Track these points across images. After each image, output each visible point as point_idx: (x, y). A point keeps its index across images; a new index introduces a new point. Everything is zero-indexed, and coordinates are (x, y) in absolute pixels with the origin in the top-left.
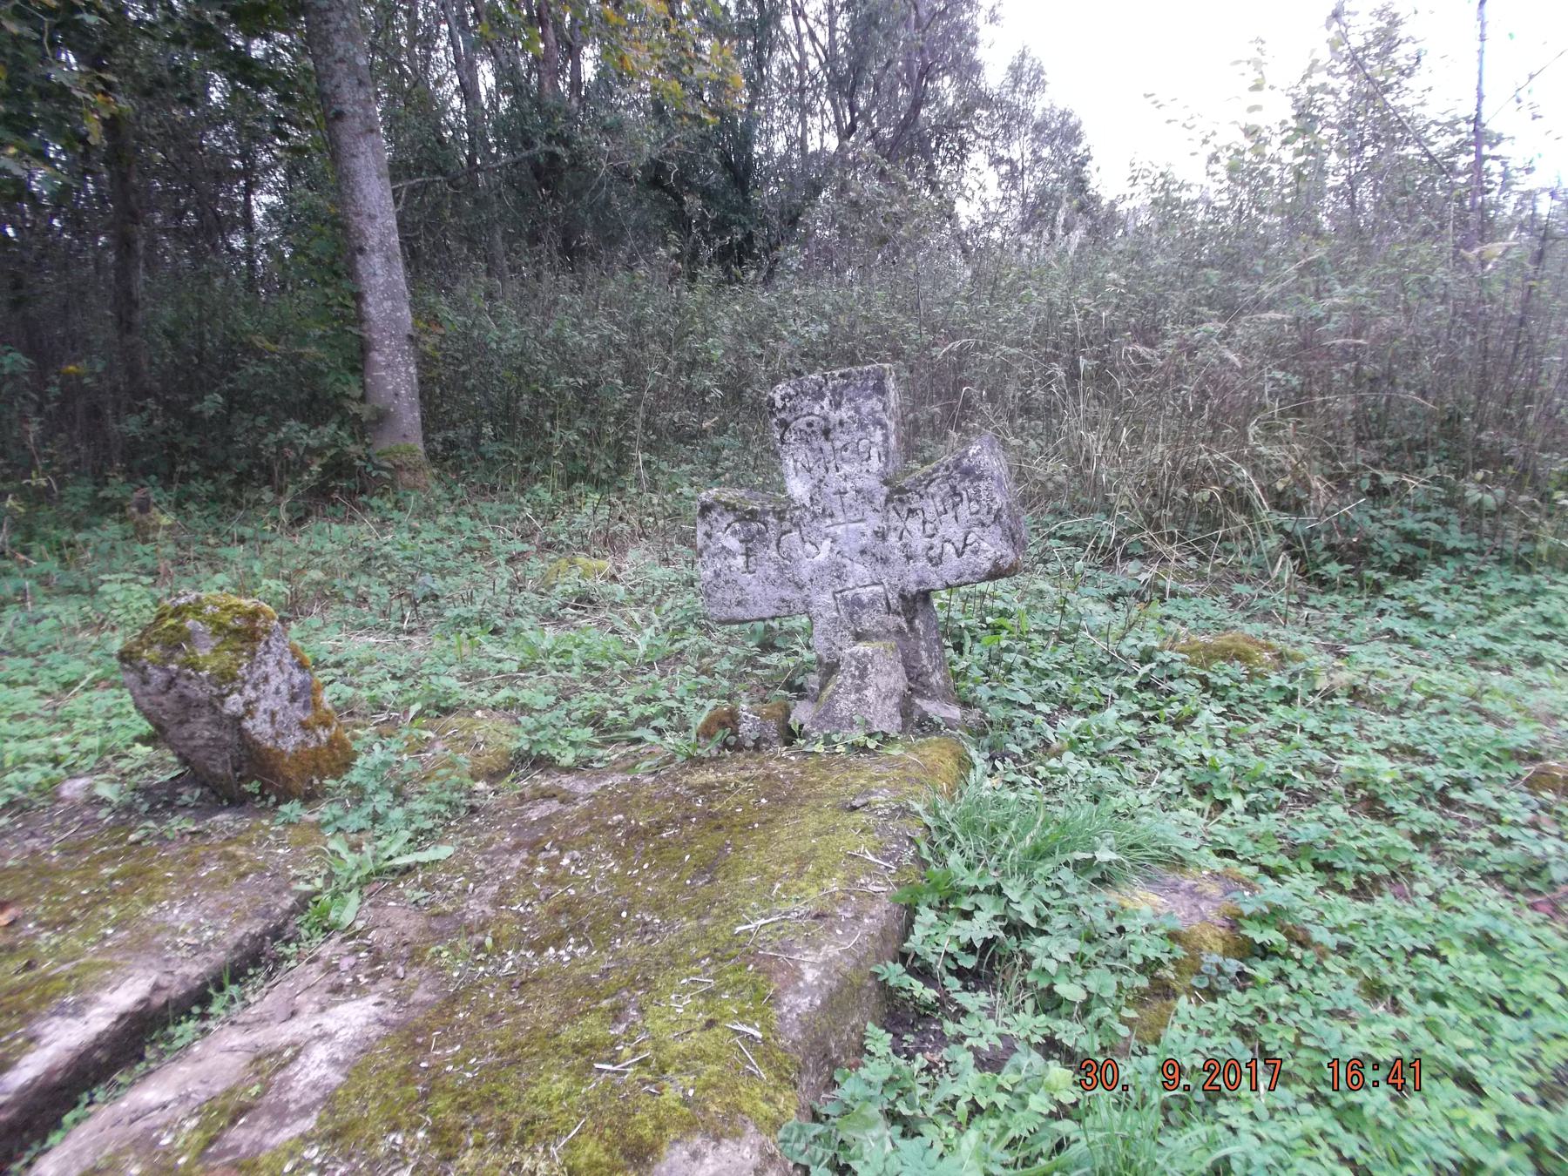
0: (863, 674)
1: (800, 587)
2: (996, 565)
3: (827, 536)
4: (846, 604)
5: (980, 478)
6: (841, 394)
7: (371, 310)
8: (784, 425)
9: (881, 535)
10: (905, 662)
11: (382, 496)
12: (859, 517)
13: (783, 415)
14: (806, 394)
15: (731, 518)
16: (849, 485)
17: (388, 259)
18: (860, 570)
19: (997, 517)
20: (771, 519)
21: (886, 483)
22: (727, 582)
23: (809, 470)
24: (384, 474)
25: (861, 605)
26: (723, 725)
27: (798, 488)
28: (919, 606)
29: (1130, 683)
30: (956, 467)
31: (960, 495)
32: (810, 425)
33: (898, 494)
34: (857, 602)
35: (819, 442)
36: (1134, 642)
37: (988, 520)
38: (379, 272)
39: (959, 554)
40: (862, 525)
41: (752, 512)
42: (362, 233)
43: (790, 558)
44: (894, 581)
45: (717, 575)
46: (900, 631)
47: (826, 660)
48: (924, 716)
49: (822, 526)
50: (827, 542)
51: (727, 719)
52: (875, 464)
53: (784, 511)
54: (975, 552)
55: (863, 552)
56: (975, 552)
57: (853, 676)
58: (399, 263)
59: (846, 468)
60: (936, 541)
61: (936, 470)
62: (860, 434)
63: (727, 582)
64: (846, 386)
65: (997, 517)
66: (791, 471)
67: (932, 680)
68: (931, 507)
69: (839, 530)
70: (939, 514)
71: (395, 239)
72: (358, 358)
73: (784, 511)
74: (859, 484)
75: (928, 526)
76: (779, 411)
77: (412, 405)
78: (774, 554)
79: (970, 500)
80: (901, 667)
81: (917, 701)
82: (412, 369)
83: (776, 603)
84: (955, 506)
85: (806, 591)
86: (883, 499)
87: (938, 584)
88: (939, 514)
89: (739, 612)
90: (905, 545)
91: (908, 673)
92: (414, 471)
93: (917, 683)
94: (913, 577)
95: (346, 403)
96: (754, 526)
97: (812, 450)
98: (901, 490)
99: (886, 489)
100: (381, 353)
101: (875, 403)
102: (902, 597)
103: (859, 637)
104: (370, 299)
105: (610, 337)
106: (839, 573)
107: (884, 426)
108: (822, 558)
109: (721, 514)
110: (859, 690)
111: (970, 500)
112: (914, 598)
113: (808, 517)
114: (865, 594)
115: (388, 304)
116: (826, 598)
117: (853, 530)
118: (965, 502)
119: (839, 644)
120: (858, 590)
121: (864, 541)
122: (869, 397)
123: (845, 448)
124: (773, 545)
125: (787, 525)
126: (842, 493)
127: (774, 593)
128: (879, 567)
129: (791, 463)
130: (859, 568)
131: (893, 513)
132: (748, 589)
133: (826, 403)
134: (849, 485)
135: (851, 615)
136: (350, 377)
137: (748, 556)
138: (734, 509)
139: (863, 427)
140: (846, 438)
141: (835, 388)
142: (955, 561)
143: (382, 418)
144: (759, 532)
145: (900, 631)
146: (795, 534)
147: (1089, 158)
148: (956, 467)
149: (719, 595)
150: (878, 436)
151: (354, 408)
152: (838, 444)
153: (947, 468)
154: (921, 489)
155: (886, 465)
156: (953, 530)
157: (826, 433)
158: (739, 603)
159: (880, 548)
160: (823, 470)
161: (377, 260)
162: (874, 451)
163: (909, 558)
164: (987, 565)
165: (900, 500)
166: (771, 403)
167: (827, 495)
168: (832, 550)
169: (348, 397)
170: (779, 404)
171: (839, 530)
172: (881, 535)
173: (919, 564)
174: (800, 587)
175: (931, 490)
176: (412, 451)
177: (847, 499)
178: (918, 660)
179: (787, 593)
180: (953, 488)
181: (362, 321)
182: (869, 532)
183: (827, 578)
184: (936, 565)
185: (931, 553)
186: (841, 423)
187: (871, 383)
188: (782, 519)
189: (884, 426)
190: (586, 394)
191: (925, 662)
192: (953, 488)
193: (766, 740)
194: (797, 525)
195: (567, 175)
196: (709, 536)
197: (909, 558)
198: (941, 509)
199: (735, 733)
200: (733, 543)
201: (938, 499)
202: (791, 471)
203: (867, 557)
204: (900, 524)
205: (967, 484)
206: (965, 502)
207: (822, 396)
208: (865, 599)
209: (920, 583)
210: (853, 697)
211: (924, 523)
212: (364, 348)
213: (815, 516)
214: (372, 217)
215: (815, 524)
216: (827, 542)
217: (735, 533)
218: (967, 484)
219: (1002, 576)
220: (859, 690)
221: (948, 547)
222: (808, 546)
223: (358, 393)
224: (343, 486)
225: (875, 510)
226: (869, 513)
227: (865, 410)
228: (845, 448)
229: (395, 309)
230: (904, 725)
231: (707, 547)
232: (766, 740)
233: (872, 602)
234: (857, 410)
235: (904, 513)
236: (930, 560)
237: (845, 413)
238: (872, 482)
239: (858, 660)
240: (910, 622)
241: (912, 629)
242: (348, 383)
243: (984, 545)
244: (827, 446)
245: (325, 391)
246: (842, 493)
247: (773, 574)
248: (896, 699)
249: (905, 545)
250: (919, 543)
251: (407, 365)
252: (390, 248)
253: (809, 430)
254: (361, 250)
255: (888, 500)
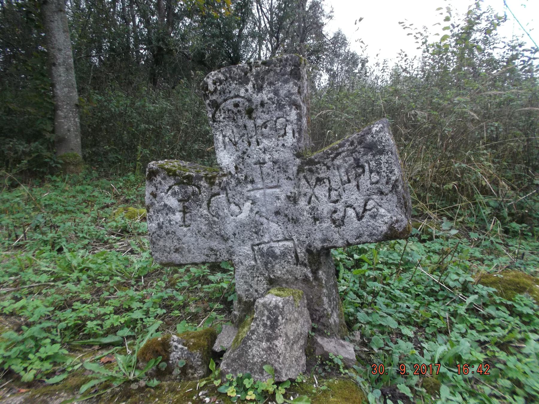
0: (274, 325)
1: (225, 239)
2: (391, 228)
3: (248, 199)
4: (262, 255)
5: (382, 152)
6: (263, 79)
7: (58, 91)
8: (216, 105)
9: (293, 199)
10: (309, 307)
11: (57, 176)
12: (274, 184)
13: (214, 97)
14: (233, 79)
15: (172, 182)
16: (267, 157)
17: (67, 70)
18: (274, 228)
19: (395, 186)
20: (203, 183)
21: (298, 155)
22: (167, 233)
23: (235, 144)
24: (59, 166)
25: (275, 256)
26: (157, 353)
27: (225, 158)
28: (322, 259)
29: (462, 310)
30: (360, 143)
31: (363, 167)
32: (236, 105)
33: (308, 166)
34: (271, 254)
35: (243, 120)
36: (455, 277)
37: (386, 189)
38: (62, 75)
39: (360, 218)
40: (277, 190)
41: (189, 178)
42: (55, 56)
43: (218, 215)
44: (303, 238)
45: (160, 227)
46: (306, 280)
47: (245, 299)
48: (325, 356)
49: (245, 191)
50: (248, 204)
51: (159, 348)
52: (290, 140)
53: (214, 177)
54: (374, 217)
55: (277, 213)
56: (374, 217)
57: (265, 325)
58: (73, 72)
59: (265, 143)
60: (340, 206)
61: (341, 146)
62: (279, 113)
63: (167, 233)
64: (268, 72)
65: (395, 186)
66: (220, 144)
67: (331, 321)
68: (337, 177)
69: (258, 194)
70: (343, 183)
71: (71, 61)
72: (51, 112)
73: (214, 177)
74: (276, 156)
75: (333, 193)
76: (212, 93)
77: (76, 135)
78: (205, 212)
79: (371, 172)
80: (306, 312)
81: (319, 340)
82: (77, 120)
83: (206, 252)
84: (358, 176)
85: (230, 243)
86: (295, 169)
87: (340, 243)
88: (343, 183)
89: (176, 258)
90: (313, 209)
91: (311, 315)
92: (76, 165)
93: (319, 325)
94: (319, 236)
95: (44, 133)
96: (190, 189)
97: (238, 127)
98: (311, 162)
99: (298, 161)
100: (62, 111)
101: (291, 87)
102: (309, 251)
103: (272, 282)
104: (58, 87)
105: (166, 108)
106: (257, 229)
107: (298, 107)
108: (243, 216)
109: (164, 179)
110: (270, 339)
111: (371, 172)
112: (319, 252)
113: (233, 182)
114: (278, 247)
115: (66, 90)
116: (246, 249)
117: (270, 194)
118: (367, 173)
119: (255, 287)
120: (272, 244)
121: (278, 204)
122: (286, 82)
123: (265, 125)
124: (204, 205)
125: (216, 189)
126: (261, 163)
127: (204, 243)
128: (290, 226)
129: (221, 138)
130: (274, 226)
131: (303, 181)
132: (184, 240)
133: (250, 86)
134: (267, 157)
135: (266, 264)
136: (48, 122)
137: (185, 213)
138: (175, 175)
139: (280, 107)
140: (266, 116)
141: (258, 73)
142: (356, 224)
143: (62, 141)
144: (194, 193)
145: (306, 280)
146: (223, 196)
147: (367, 61)
148: (360, 143)
149: (161, 243)
150: (293, 115)
151: (48, 136)
152: (259, 122)
153: (352, 144)
154: (328, 162)
155: (299, 141)
156: (354, 197)
157: (250, 112)
158: (177, 250)
159: (291, 211)
160: (246, 144)
161: (61, 69)
162: (289, 129)
163: (316, 219)
164: (384, 228)
165: (310, 170)
166: (206, 85)
167: (249, 165)
168: (251, 210)
169: (45, 130)
170: (211, 87)
171: (258, 194)
172: (293, 199)
173: (325, 225)
174: (225, 239)
175: (338, 162)
176: (75, 156)
177: (266, 168)
178: (320, 303)
179: (214, 244)
180: (357, 160)
181: (54, 96)
182: (283, 197)
183: (247, 234)
184: (339, 226)
185: (335, 216)
186: (262, 104)
187: (289, 69)
188: (212, 184)
189: (298, 107)
190: (158, 133)
191: (326, 306)
192: (357, 160)
193: (191, 367)
194: (224, 189)
195: (166, 56)
196: (154, 195)
197: (316, 219)
198: (345, 178)
199: (167, 360)
200: (173, 202)
201: (343, 170)
202: (220, 144)
203: (281, 218)
204: (309, 191)
205: (370, 157)
206: (367, 173)
207: (247, 82)
208: (278, 252)
209: (324, 241)
210: (264, 345)
211: (330, 190)
212: (55, 109)
213: (239, 182)
214: (60, 50)
215: (239, 189)
216: (248, 204)
217: (174, 194)
218: (370, 157)
219: (396, 238)
220: (270, 339)
221: (350, 211)
222: (233, 207)
223: (51, 129)
224: (39, 171)
225: (288, 178)
226: (283, 181)
227: (283, 92)
228: (265, 125)
229: (69, 92)
230: (309, 364)
231: (152, 204)
232: (191, 367)
233: (284, 254)
234: (276, 93)
235: (313, 181)
236: (334, 221)
237: (265, 95)
238: (286, 155)
239: (269, 311)
240: (314, 273)
241: (316, 278)
242: (46, 124)
243: (382, 211)
244: (250, 124)
245: (38, 128)
246: (261, 163)
247: (204, 228)
248: (302, 342)
249: (313, 209)
250: (325, 207)
251: (74, 118)
252: (69, 64)
253: (235, 110)
254: (54, 65)
255: (300, 170)
